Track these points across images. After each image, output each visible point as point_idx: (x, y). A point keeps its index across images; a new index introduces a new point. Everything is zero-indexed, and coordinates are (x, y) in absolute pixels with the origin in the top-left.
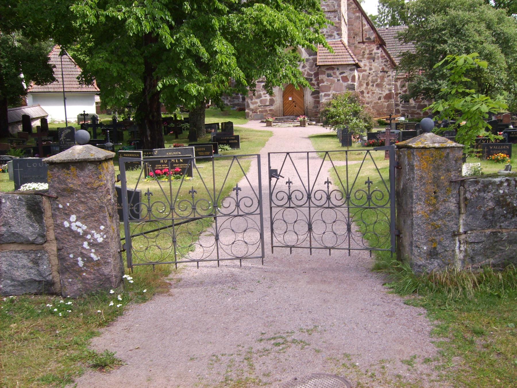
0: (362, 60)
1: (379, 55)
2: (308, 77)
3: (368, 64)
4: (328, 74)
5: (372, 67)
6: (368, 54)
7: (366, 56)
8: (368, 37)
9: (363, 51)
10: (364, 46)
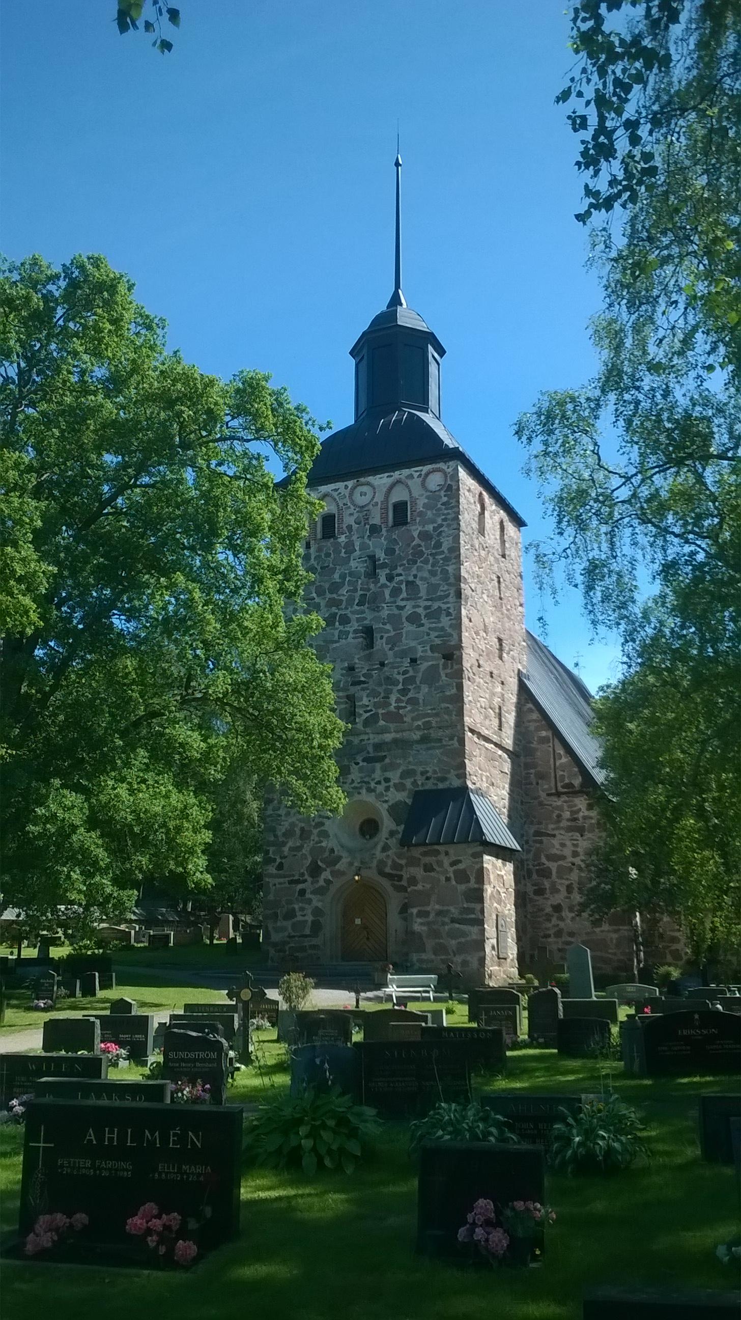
2: (394, 872)
4: (425, 865)
5: (579, 849)
6: (568, 820)
8: (567, 781)
10: (559, 803)
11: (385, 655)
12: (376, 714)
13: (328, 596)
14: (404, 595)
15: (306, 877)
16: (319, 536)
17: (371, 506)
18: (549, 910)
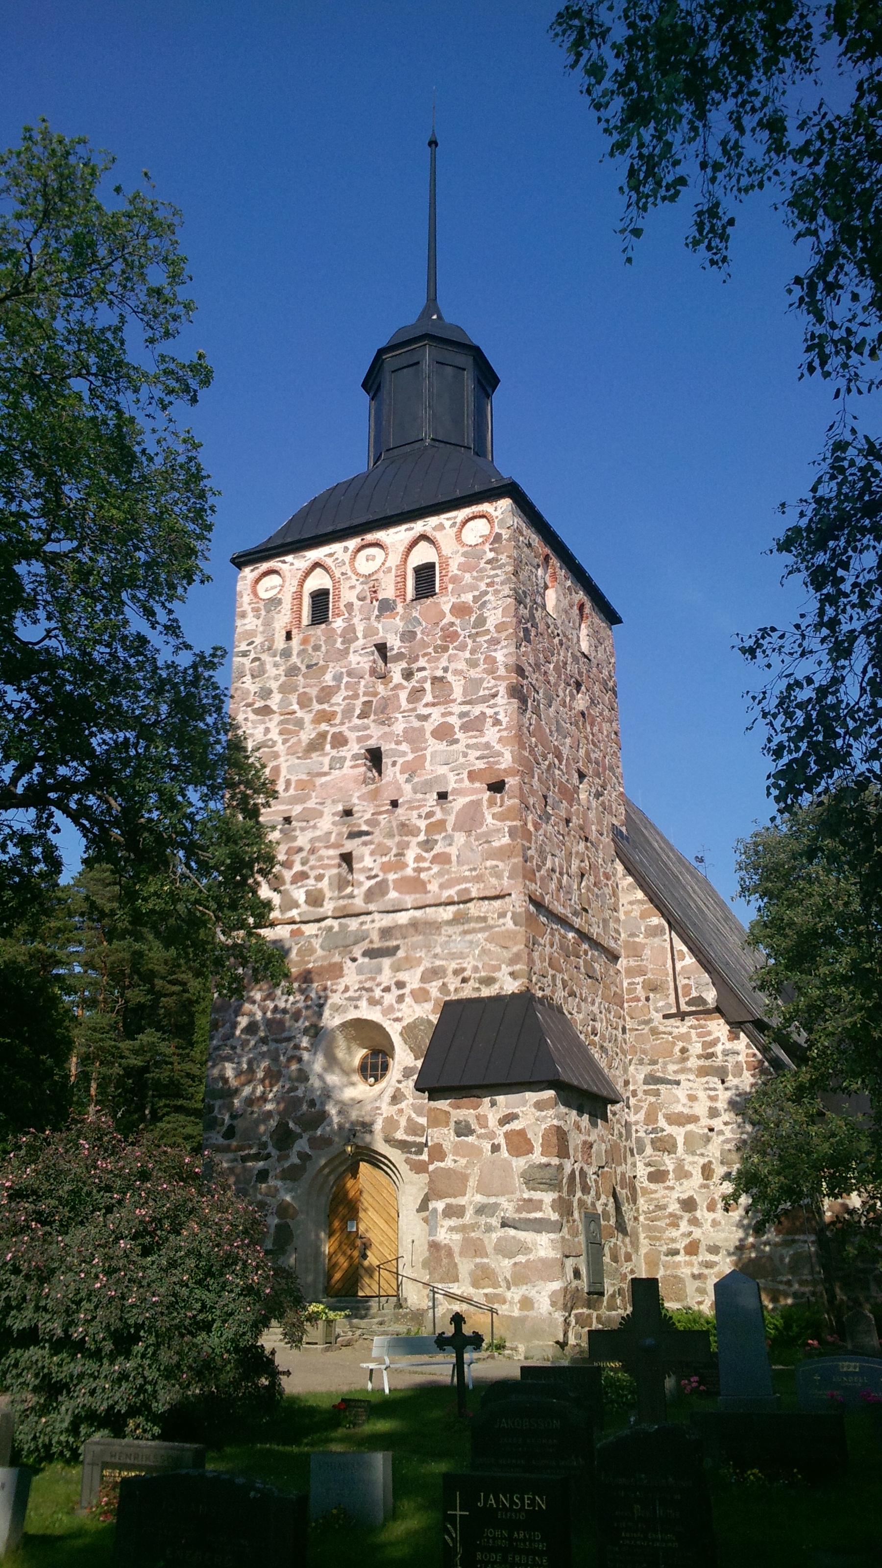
0: (681, 1077)
1: (741, 1058)
2: (410, 1139)
3: (702, 1095)
6: (699, 1057)
7: (693, 1063)
8: (694, 994)
9: (680, 1044)
10: (683, 1030)
11: (399, 789)
12: (384, 881)
13: (317, 707)
14: (428, 698)
15: (270, 1149)
16: (306, 619)
17: (381, 575)
18: (674, 1207)
